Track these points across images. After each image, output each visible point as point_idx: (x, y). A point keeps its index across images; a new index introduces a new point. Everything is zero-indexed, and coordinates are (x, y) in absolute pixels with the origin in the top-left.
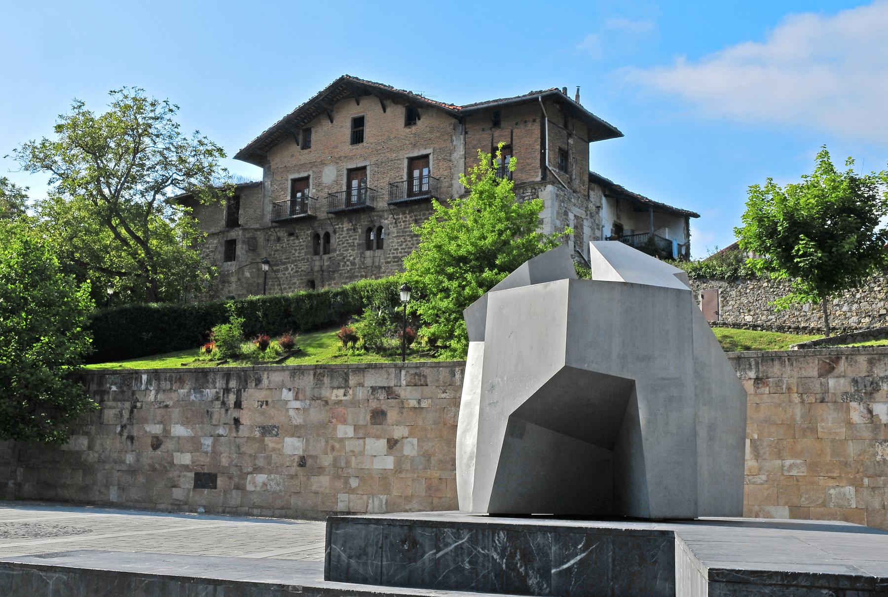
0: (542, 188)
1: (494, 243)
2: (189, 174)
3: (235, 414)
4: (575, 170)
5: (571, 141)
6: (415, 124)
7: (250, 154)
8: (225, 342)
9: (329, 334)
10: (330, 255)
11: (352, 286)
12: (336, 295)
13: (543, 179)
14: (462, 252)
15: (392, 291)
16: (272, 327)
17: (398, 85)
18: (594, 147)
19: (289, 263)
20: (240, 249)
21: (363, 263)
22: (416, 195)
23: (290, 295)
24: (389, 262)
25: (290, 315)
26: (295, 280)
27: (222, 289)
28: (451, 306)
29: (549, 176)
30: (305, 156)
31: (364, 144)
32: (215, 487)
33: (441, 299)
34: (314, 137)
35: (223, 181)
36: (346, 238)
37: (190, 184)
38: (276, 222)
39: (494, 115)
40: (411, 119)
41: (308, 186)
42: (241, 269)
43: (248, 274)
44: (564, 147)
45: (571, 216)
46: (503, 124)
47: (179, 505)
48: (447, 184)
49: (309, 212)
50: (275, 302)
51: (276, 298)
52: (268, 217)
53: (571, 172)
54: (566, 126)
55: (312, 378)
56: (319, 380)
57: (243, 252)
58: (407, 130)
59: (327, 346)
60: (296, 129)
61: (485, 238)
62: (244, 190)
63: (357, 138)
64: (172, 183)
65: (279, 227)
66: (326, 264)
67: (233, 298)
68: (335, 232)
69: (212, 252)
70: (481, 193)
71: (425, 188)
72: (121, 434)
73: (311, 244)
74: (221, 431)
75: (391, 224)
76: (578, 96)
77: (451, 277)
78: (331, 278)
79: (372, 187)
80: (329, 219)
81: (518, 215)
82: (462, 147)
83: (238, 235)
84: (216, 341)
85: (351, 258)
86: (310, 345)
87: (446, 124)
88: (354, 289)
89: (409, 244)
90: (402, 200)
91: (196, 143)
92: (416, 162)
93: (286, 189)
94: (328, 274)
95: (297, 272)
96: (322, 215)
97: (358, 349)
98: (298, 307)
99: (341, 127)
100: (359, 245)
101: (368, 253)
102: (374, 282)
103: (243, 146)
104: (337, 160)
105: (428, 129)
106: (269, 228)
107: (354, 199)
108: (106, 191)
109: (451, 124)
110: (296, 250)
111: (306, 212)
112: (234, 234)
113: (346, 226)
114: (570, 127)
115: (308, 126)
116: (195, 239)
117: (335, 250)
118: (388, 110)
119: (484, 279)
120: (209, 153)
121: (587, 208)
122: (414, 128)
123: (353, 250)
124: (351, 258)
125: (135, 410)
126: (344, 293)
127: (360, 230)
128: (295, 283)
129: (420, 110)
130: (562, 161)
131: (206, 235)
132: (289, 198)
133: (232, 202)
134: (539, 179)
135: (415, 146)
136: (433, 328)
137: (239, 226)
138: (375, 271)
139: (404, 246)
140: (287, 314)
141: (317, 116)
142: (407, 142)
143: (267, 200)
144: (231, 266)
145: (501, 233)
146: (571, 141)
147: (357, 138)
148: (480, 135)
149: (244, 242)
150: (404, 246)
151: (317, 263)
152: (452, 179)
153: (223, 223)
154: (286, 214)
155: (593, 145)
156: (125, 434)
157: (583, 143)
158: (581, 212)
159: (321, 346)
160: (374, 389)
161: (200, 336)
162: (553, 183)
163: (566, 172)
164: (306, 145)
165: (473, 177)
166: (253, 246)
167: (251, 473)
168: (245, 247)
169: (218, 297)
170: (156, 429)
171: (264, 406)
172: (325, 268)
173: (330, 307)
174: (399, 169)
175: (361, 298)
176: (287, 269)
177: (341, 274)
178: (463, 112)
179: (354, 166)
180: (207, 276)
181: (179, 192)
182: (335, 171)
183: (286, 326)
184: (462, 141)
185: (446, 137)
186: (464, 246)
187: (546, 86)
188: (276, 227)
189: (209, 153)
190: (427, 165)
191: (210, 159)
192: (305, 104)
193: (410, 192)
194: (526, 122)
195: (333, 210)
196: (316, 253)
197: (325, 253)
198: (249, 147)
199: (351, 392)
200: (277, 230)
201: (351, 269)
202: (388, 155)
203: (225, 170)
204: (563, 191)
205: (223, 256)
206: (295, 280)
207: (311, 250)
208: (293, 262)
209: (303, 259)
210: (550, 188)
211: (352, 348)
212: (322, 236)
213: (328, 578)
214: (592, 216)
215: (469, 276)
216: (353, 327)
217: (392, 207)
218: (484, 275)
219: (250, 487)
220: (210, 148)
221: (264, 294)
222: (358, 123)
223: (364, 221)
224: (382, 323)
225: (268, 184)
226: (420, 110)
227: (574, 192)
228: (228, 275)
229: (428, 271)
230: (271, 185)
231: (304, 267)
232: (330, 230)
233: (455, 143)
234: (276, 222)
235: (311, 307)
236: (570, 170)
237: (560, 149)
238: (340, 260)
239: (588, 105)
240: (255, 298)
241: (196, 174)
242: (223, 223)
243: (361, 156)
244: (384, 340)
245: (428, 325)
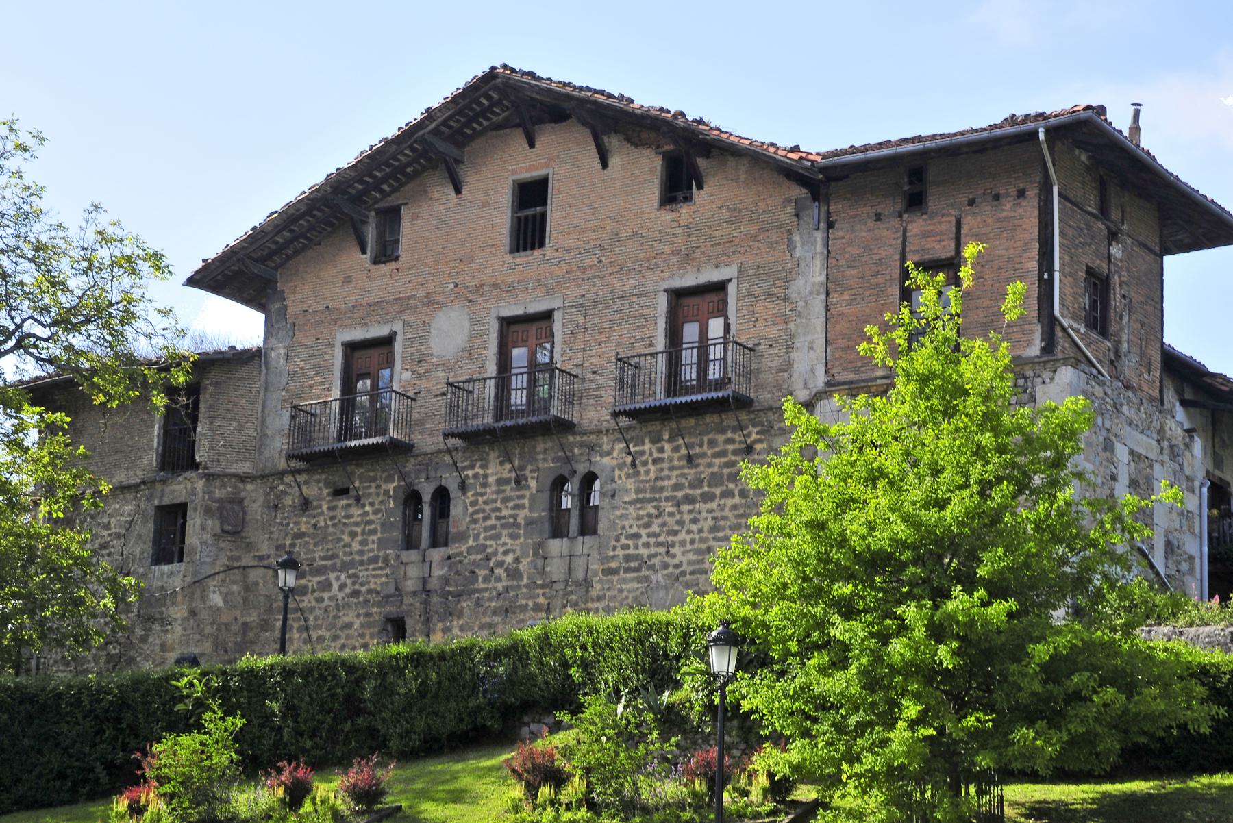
0: (1046, 375)
1: (970, 515)
2: (66, 321)
4: (1126, 328)
5: (1116, 251)
6: (688, 199)
7: (225, 276)
8: (186, 782)
9: (472, 764)
10: (450, 550)
11: (538, 630)
12: (494, 656)
13: (1043, 350)
14: (881, 540)
15: (654, 647)
16: (309, 744)
17: (647, 93)
18: (1180, 269)
19: (333, 568)
20: (198, 531)
21: (543, 573)
22: (689, 390)
23: (361, 654)
24: (614, 572)
25: (359, 712)
26: (348, 617)
27: (144, 639)
28: (854, 689)
29: (1062, 343)
30: (383, 282)
31: (548, 250)
33: (822, 670)
34: (406, 229)
35: (159, 341)
36: (495, 505)
37: (69, 348)
38: (300, 457)
39: (911, 176)
40: (678, 184)
41: (390, 363)
42: (198, 584)
43: (216, 599)
44: (1101, 266)
45: (1122, 453)
46: (932, 203)
48: (777, 362)
49: (393, 433)
50: (319, 672)
51: (322, 663)
52: (278, 445)
53: (1118, 334)
54: (1104, 212)
57: (207, 537)
58: (667, 216)
59: (475, 800)
60: (359, 206)
61: (942, 504)
62: (219, 366)
63: (529, 234)
64: (18, 345)
65: (307, 471)
66: (437, 573)
67: (194, 661)
68: (463, 487)
69: (118, 536)
70: (924, 380)
71: (714, 372)
73: (397, 518)
75: (621, 466)
76: (1135, 129)
77: (848, 610)
78: (449, 613)
79: (568, 368)
80: (449, 451)
81: (1028, 439)
82: (818, 263)
83: (193, 492)
84: (162, 780)
85: (509, 559)
86: (425, 795)
87: (778, 200)
88: (544, 639)
89: (671, 521)
90: (653, 403)
91: (91, 238)
92: (519, 328)
93: (329, 368)
94: (441, 601)
95: (355, 593)
96: (428, 440)
97: (569, 807)
98: (385, 690)
99: (485, 205)
100: (530, 523)
101: (555, 546)
102: (600, 621)
103: (213, 250)
104: (471, 294)
105: (725, 214)
106: (281, 474)
107: (518, 398)
109: (787, 201)
110: (353, 535)
111: (384, 431)
112: (180, 488)
113: (496, 469)
114: (1115, 214)
116: (75, 500)
117: (463, 537)
118: (615, 161)
119: (951, 617)
120: (129, 265)
121: (1161, 431)
122: (685, 211)
123: (513, 537)
124: (509, 559)
126: (515, 650)
127: (533, 484)
128: (349, 626)
129: (701, 163)
130: (1093, 303)
131: (105, 487)
132: (336, 393)
133: (183, 400)
134: (1034, 350)
135: (687, 258)
136: (796, 753)
137: (195, 466)
138: (579, 591)
139: (655, 528)
140: (353, 705)
141: (416, 174)
142: (667, 249)
143: (274, 398)
144: (172, 576)
145: (985, 488)
146: (1116, 251)
147: (529, 234)
148: (873, 234)
149: (208, 511)
150: (655, 528)
151: (413, 572)
152: (790, 349)
153: (153, 458)
154: (328, 438)
155: (1174, 264)
157: (1149, 258)
158: (1146, 445)
159: (457, 797)
161: (99, 768)
162: (1075, 364)
163: (1104, 333)
164: (386, 253)
165: (900, 336)
166: (232, 522)
168: (213, 524)
169: (132, 661)
172: (434, 584)
173: (475, 688)
174: (646, 320)
175: (566, 665)
176: (327, 586)
177: (478, 603)
178: (823, 170)
179: (519, 311)
180: (108, 602)
181: (32, 370)
182: (467, 324)
183: (347, 741)
184: (820, 248)
185: (774, 236)
186: (878, 522)
187: (1058, 98)
188: (299, 472)
189: (129, 265)
190: (722, 311)
191: (126, 281)
192: (388, 143)
193: (674, 384)
194: (997, 197)
195: (461, 426)
196: (410, 543)
197: (434, 544)
198: (231, 255)
200: (301, 478)
201: (507, 589)
202: (615, 282)
203: (166, 313)
204: (1101, 384)
205: (149, 548)
206: (348, 617)
207: (397, 534)
208: (345, 567)
209: (374, 560)
210: (1066, 374)
211: (552, 803)
212: (427, 498)
214: (1174, 455)
215: (909, 611)
216: (550, 743)
217: (624, 421)
218: (950, 606)
220: (128, 251)
221: (283, 650)
222: (532, 194)
223: (546, 457)
224: (629, 737)
225: (277, 354)
226: (701, 163)
227: (1128, 387)
228: (162, 601)
229: (781, 590)
230: (288, 358)
231: (377, 580)
232: (450, 481)
233: (798, 252)
234: (300, 457)
235: (423, 691)
236: (1113, 328)
237: (1090, 272)
238: (477, 564)
239: (1174, 148)
240: (261, 663)
241: (88, 321)
242: (152, 458)
243: (538, 284)
244: (643, 783)
245: (781, 741)
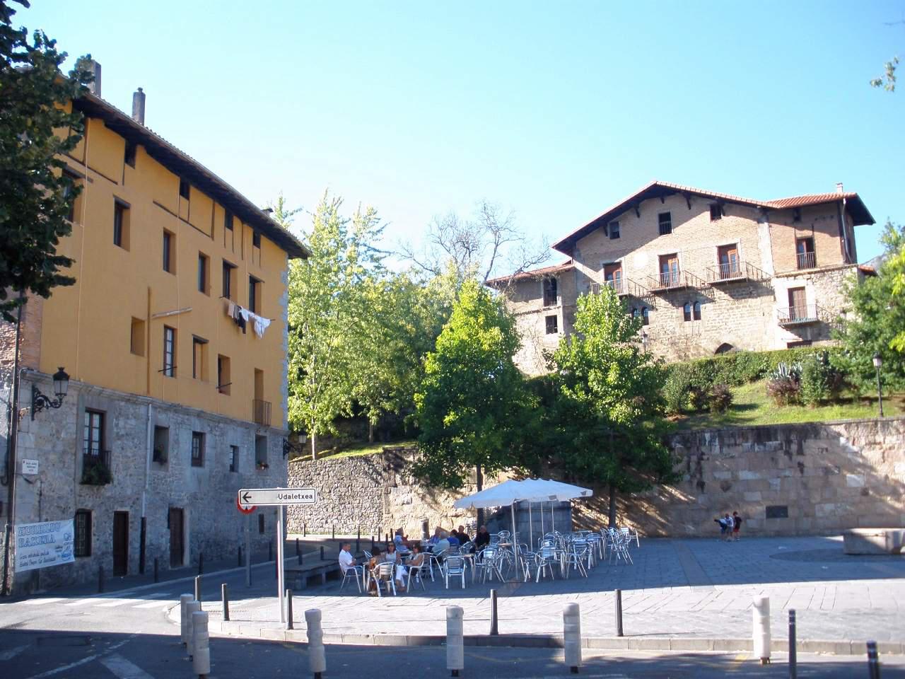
3: (800, 459)
32: (787, 516)
34: (621, 230)
47: (754, 532)
58: (714, 224)
72: (690, 482)
74: (787, 473)
124: (671, 328)
125: (702, 462)
156: (695, 482)
167: (820, 503)
170: (726, 476)
171: (824, 452)
194: (824, 218)
213: (490, 597)
219: (819, 514)
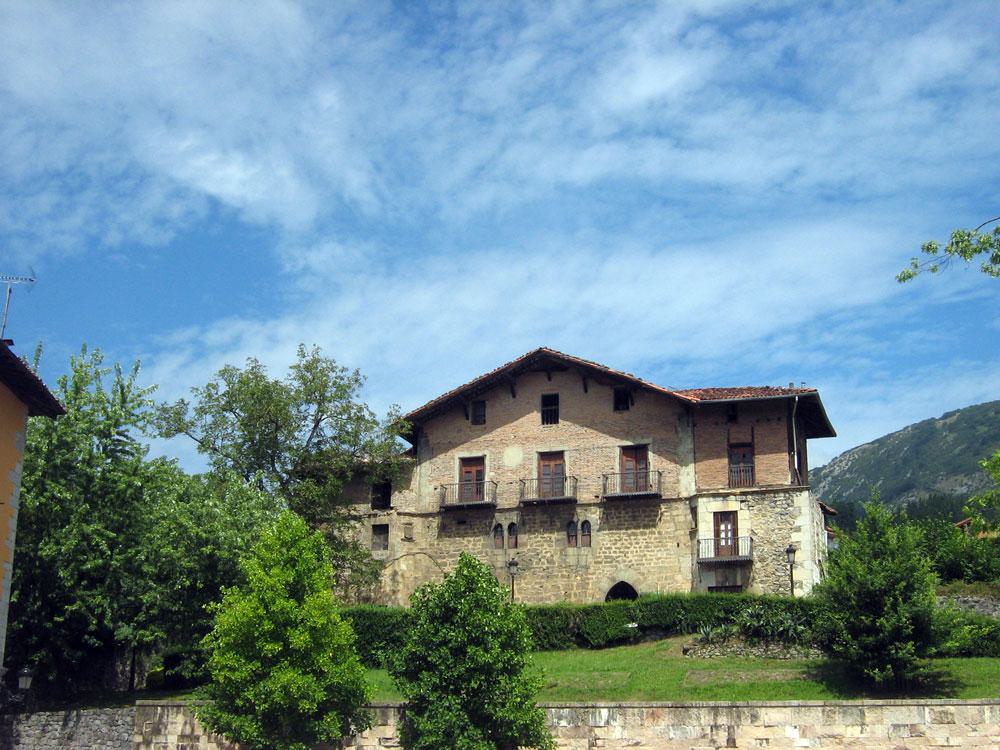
10: (756, 559)
34: (489, 412)
46: (740, 419)
55: (821, 715)
56: (828, 716)
85: (548, 555)
89: (626, 543)
93: (452, 468)
101: (571, 551)
108: (287, 455)
111: (483, 499)
115: (480, 398)
124: (548, 555)
150: (618, 545)
160: (896, 727)
177: (534, 573)
199: (868, 729)
201: (548, 568)
